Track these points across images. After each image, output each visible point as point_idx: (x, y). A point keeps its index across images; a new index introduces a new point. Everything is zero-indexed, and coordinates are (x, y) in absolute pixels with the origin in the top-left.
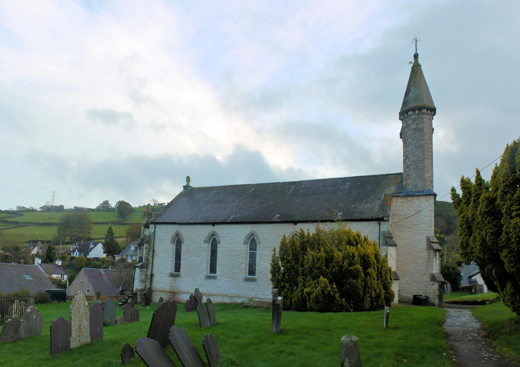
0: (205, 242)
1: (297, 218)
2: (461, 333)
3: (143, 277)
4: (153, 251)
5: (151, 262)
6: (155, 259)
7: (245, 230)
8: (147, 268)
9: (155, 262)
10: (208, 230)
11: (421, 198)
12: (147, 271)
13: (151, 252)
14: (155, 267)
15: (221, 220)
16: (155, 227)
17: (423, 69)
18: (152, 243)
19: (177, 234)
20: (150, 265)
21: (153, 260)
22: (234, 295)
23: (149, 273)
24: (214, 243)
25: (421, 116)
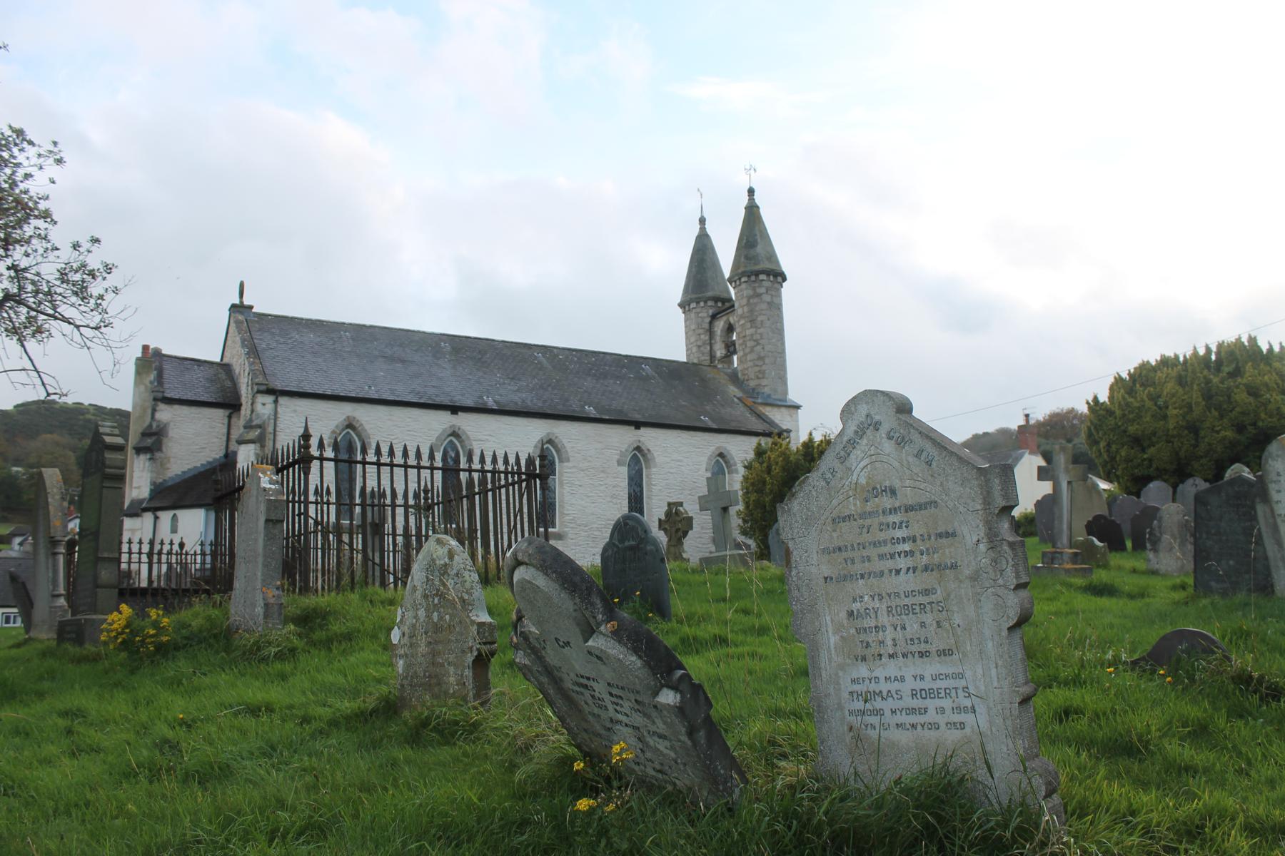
1: (638, 417)
11: (783, 409)
15: (469, 402)
16: (276, 402)
19: (350, 425)
24: (637, 462)
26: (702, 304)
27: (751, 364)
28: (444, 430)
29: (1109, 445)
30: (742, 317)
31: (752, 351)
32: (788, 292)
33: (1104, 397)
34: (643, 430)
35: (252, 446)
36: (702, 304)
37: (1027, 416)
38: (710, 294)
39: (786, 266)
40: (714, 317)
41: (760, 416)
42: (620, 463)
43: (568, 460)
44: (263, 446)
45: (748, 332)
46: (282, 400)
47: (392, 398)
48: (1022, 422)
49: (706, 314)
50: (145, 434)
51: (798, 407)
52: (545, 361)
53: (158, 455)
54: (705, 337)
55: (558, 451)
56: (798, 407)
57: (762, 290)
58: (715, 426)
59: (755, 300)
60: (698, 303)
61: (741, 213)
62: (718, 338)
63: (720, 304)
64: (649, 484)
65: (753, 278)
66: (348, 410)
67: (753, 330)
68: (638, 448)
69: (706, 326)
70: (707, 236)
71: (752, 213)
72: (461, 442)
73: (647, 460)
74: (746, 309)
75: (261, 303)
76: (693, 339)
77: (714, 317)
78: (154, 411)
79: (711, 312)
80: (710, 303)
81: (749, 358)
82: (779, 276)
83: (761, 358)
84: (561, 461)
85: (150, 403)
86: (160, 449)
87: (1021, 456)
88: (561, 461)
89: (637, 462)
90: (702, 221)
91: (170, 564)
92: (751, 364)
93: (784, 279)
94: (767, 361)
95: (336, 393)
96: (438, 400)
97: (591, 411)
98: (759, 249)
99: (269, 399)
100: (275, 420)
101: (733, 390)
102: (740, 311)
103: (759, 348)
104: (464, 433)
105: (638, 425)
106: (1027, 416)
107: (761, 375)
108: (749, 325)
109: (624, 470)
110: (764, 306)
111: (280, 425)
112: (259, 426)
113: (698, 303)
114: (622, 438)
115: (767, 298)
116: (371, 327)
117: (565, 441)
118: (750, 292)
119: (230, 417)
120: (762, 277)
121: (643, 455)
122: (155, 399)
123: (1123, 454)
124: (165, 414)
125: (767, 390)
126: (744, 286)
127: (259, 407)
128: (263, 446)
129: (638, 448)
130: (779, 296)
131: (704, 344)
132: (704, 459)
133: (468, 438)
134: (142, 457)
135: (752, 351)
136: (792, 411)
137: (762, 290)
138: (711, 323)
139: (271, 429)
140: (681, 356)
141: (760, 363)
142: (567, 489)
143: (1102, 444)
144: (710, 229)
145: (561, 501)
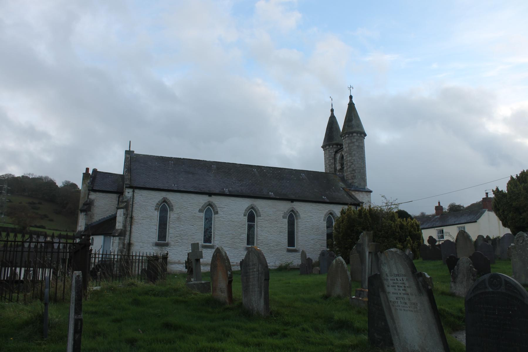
0: (201, 211)
1: (293, 197)
2: (430, 287)
3: (121, 246)
4: (132, 218)
5: (128, 229)
6: (133, 227)
7: (244, 204)
8: (125, 237)
9: (133, 230)
10: (203, 200)
11: (364, 193)
12: (124, 239)
13: (128, 219)
14: (133, 235)
15: (217, 191)
16: (133, 191)
17: (356, 106)
18: (130, 209)
19: (165, 201)
20: (128, 233)
21: (131, 228)
22: (235, 264)
23: (126, 241)
24: (292, 219)
25: (361, 138)
26: (331, 147)
27: (349, 173)
28: (205, 203)
29: (503, 211)
30: (346, 152)
31: (350, 167)
32: (366, 140)
33: (504, 188)
34: (295, 203)
35: (122, 210)
36: (331, 147)
37: (487, 194)
38: (334, 142)
39: (366, 129)
40: (336, 152)
41: (351, 196)
42: (284, 217)
43: (260, 216)
44: (127, 210)
45: (348, 159)
46: (136, 191)
47: (183, 189)
48: (485, 197)
49: (332, 151)
50: (85, 204)
51: (371, 192)
52: (257, 172)
53: (89, 213)
54: (332, 161)
55: (256, 212)
56: (371, 192)
57: (355, 140)
58: (328, 201)
59: (352, 145)
60: (329, 146)
61: (346, 107)
62: (338, 161)
63: (339, 147)
64: (297, 227)
65: (351, 135)
66: (164, 195)
67: (350, 158)
68: (292, 211)
69: (333, 156)
70: (334, 117)
71: (351, 107)
72: (213, 208)
73: (296, 216)
74: (347, 149)
75: (138, 150)
76: (327, 162)
77: (336, 152)
78: (89, 195)
79: (335, 150)
80: (334, 146)
81: (349, 170)
82: (365, 135)
83: (354, 170)
84: (257, 217)
85: (87, 192)
86: (90, 210)
87: (484, 212)
88: (257, 217)
89: (292, 219)
90: (332, 110)
91: (102, 258)
92: (349, 173)
93: (365, 135)
94: (356, 171)
95: (159, 187)
96: (203, 190)
97: (271, 194)
98: (353, 122)
99: (131, 190)
100: (133, 199)
101: (341, 184)
102: (345, 150)
103: (353, 166)
104: (214, 204)
105: (292, 201)
106: (487, 194)
107: (354, 177)
108: (349, 156)
109: (286, 221)
110: (355, 147)
111: (135, 201)
112: (126, 202)
113: (329, 146)
114: (284, 207)
115: (357, 144)
116: (184, 159)
117: (259, 208)
118: (349, 141)
119: (119, 197)
120: (355, 134)
121: (295, 214)
122: (89, 190)
123: (510, 215)
124: (93, 196)
125: (356, 184)
126: (347, 139)
127: (131, 194)
128: (127, 210)
129: (292, 211)
130: (363, 143)
131: (332, 164)
132: (323, 216)
133: (216, 206)
134: (83, 214)
135: (350, 167)
136: (368, 193)
137: (355, 140)
138: (335, 155)
139: (131, 203)
140: (321, 169)
141: (354, 172)
142: (259, 229)
143: (501, 211)
144: (335, 114)
145: (257, 234)
